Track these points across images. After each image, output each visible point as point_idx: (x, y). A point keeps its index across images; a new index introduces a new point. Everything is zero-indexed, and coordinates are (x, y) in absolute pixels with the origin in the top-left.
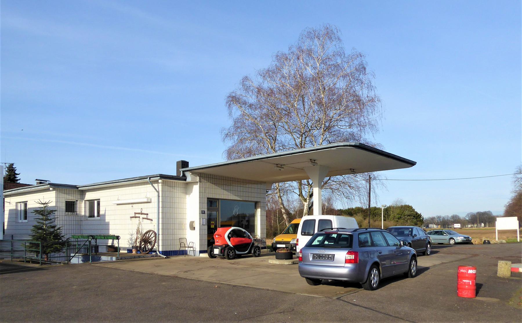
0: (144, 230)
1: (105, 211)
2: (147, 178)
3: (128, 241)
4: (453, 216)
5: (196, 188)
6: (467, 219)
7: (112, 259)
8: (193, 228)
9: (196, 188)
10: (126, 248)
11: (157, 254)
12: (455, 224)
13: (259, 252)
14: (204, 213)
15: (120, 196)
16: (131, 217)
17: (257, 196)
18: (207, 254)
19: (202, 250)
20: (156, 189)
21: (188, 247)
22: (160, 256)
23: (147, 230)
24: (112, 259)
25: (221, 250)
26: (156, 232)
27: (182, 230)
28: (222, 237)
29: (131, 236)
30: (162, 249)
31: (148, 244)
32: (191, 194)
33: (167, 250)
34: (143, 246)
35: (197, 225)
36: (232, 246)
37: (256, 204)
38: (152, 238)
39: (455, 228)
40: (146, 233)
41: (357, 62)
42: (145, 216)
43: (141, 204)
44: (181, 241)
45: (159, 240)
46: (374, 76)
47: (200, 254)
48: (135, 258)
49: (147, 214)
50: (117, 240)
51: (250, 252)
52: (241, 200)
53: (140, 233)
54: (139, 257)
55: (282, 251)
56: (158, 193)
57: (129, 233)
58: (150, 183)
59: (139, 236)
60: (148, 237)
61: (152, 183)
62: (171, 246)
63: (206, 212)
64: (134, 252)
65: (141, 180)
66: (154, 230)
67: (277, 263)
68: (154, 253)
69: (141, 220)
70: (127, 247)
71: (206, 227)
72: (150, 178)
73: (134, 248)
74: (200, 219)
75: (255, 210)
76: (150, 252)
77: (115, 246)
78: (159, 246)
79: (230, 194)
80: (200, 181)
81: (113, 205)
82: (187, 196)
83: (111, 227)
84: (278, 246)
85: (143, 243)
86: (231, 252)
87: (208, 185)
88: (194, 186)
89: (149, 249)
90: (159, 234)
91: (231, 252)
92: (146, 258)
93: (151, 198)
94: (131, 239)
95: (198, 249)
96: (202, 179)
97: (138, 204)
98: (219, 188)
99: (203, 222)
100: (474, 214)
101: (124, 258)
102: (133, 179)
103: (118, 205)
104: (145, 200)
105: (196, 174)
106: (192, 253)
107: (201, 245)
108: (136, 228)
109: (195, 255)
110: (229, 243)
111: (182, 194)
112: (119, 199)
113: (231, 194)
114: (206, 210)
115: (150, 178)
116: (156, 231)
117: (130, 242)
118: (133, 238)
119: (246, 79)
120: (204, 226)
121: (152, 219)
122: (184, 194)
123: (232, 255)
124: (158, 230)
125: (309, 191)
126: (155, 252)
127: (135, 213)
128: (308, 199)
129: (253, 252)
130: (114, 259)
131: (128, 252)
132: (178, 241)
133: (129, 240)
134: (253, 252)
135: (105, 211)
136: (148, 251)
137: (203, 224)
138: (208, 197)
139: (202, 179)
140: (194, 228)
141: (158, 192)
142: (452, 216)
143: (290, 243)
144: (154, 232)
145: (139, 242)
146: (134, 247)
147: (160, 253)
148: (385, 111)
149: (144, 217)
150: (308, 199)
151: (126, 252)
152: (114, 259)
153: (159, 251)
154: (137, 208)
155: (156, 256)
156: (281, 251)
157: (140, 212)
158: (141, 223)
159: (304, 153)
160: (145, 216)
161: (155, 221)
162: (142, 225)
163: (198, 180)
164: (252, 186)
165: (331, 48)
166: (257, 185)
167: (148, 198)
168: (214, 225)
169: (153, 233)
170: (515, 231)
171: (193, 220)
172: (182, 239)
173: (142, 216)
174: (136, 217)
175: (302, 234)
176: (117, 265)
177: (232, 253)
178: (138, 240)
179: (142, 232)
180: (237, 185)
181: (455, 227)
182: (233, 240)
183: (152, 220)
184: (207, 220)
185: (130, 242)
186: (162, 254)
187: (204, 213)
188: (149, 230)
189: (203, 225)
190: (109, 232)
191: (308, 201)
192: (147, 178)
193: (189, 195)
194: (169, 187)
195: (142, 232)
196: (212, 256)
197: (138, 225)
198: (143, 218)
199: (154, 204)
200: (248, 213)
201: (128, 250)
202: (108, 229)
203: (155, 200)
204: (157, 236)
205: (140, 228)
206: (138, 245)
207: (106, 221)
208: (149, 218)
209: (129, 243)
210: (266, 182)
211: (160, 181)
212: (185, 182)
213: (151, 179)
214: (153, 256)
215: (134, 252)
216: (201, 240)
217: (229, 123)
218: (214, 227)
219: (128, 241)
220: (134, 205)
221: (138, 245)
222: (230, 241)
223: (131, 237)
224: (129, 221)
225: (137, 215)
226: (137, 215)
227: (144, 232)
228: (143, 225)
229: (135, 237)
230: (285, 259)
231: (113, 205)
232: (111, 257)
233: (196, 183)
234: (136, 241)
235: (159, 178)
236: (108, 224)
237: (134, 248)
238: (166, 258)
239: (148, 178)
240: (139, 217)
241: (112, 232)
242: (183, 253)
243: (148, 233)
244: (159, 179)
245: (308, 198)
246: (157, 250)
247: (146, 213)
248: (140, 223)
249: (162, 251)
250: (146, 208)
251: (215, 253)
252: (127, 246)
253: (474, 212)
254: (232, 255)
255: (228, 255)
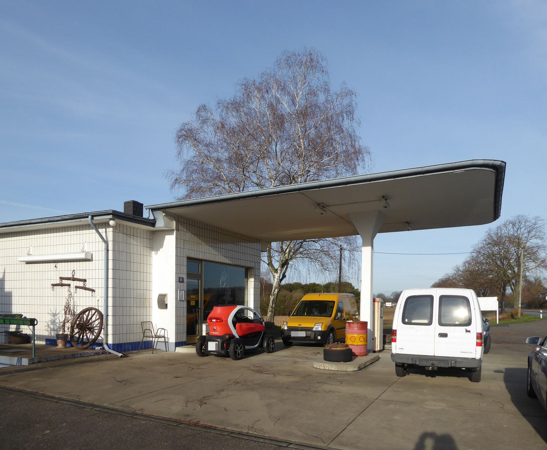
0: (78, 308)
1: (4, 273)
2: (88, 217)
3: (48, 325)
4: (379, 295)
5: (170, 241)
6: (392, 298)
7: (20, 361)
8: (162, 304)
9: (170, 241)
10: (44, 337)
11: (104, 348)
12: (386, 303)
13: (272, 345)
14: (183, 282)
15: (31, 248)
16: (54, 285)
17: (245, 258)
18: (195, 349)
19: (180, 341)
20: (102, 237)
21: (156, 337)
22: (110, 353)
23: (85, 308)
24: (20, 361)
25: (222, 344)
26: (101, 311)
27: (145, 309)
28: (223, 322)
29: (54, 316)
30: (114, 339)
31: (86, 331)
32: (161, 249)
33: (121, 342)
34: (77, 335)
35: (171, 301)
36: (238, 337)
37: (248, 271)
38: (94, 321)
39: (386, 307)
40: (84, 312)
41: (346, 102)
42: (81, 284)
43: (75, 263)
44: (145, 326)
45: (107, 325)
46: (359, 124)
47: (177, 348)
48: (65, 358)
49: (85, 281)
50: (31, 327)
51: (261, 345)
52: (231, 263)
53: (70, 313)
54: (74, 356)
55: (339, 349)
56: (106, 245)
57: (50, 312)
58: (92, 226)
59: (70, 318)
60: (87, 319)
61: (97, 226)
62: (128, 335)
63: (185, 280)
64: (60, 345)
65: (74, 221)
66: (97, 308)
67: (333, 369)
68: (98, 348)
69: (73, 290)
70: (44, 334)
71: (185, 304)
72: (93, 217)
73: (61, 338)
74: (176, 291)
75: (246, 280)
76: (90, 345)
77: (23, 333)
78: (107, 335)
79: (217, 253)
80: (177, 230)
81: (18, 262)
82: (153, 252)
83: (14, 300)
84: (294, 334)
85: (76, 330)
86: (239, 348)
87: (189, 236)
88: (166, 236)
89: (90, 341)
90: (107, 316)
91: (239, 348)
92: (87, 358)
93: (92, 253)
94: (53, 322)
95: (172, 339)
96: (180, 226)
97: (66, 263)
98: (203, 243)
99: (180, 297)
100: (398, 293)
101: (45, 360)
102: (59, 219)
103: (28, 263)
104: (82, 256)
105: (171, 216)
106: (161, 347)
107: (177, 333)
108: (64, 304)
109: (167, 350)
110: (234, 332)
111: (145, 248)
112: (31, 253)
113: (219, 254)
114: (185, 277)
115: (93, 217)
116: (103, 312)
117: (52, 327)
118: (57, 321)
119: (203, 108)
120: (182, 303)
121: (94, 289)
122: (148, 249)
123: (241, 352)
124: (105, 309)
125: (282, 259)
126: (101, 344)
127: (62, 279)
128: (280, 270)
129: (265, 344)
130: (25, 362)
131: (47, 344)
132: (140, 326)
133: (49, 323)
134: (265, 344)
135: (4, 273)
136: (89, 344)
137: (181, 299)
138: (188, 255)
139: (180, 226)
140: (166, 305)
141: (106, 242)
142: (378, 295)
143: (313, 330)
144: (97, 311)
145: (68, 329)
146: (60, 336)
147: (110, 348)
148: (374, 166)
149: (78, 285)
150: (280, 270)
151: (44, 343)
152: (25, 362)
153: (107, 344)
154: (66, 270)
155: (103, 353)
156: (335, 347)
157: (70, 276)
158: (73, 295)
159: (396, 179)
160: (81, 284)
161: (100, 293)
162: (73, 299)
163: (174, 227)
164: (222, 245)
165: (316, 80)
166: (254, 244)
167: (86, 254)
168: (194, 302)
169: (97, 313)
170: (496, 311)
171: (163, 292)
172: (144, 323)
173: (73, 284)
174: (62, 285)
175: (404, 322)
176: (34, 379)
177: (240, 349)
178: (68, 325)
179: (75, 310)
180: (213, 245)
181: (387, 305)
182: (240, 327)
183: (93, 291)
184: (186, 292)
185: (52, 327)
186: (114, 349)
187: (183, 282)
188: (88, 307)
189: (180, 300)
190: (10, 308)
191: (279, 272)
192: (88, 217)
193: (156, 252)
194: (125, 236)
195: (74, 310)
196: (203, 352)
197: (67, 298)
198: (77, 287)
199: (99, 262)
200: (236, 285)
201: (47, 340)
202: (10, 304)
203: (99, 256)
204: (104, 317)
205: (72, 303)
206: (68, 332)
207: (6, 290)
208: (87, 286)
209: (49, 329)
210: (261, 240)
211: (112, 223)
212: (151, 228)
213: (95, 218)
214: (98, 354)
215: (60, 345)
216: (177, 324)
217: (178, 167)
218: (194, 304)
219: (48, 325)
220: (59, 265)
221: (68, 332)
222: (235, 329)
223: (53, 318)
224: (49, 291)
225: (65, 282)
226: (65, 282)
227: (78, 311)
228: (75, 298)
229: (61, 318)
230: (344, 362)
231: (18, 262)
232: (18, 359)
233: (170, 232)
234: (64, 326)
235: (111, 216)
236: (9, 296)
237: (61, 338)
238: (121, 356)
239: (90, 217)
240: (69, 285)
241: (15, 310)
242: (147, 346)
243: (87, 313)
244: (111, 219)
245: (279, 269)
246: (104, 342)
247: (81, 278)
248: (70, 296)
249: (113, 345)
250: (81, 270)
251: (210, 349)
252: (46, 333)
253: (398, 292)
254: (239, 351)
255: (235, 352)
